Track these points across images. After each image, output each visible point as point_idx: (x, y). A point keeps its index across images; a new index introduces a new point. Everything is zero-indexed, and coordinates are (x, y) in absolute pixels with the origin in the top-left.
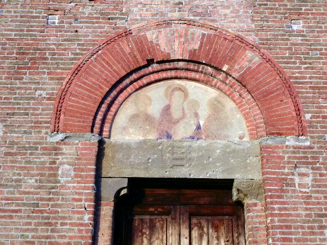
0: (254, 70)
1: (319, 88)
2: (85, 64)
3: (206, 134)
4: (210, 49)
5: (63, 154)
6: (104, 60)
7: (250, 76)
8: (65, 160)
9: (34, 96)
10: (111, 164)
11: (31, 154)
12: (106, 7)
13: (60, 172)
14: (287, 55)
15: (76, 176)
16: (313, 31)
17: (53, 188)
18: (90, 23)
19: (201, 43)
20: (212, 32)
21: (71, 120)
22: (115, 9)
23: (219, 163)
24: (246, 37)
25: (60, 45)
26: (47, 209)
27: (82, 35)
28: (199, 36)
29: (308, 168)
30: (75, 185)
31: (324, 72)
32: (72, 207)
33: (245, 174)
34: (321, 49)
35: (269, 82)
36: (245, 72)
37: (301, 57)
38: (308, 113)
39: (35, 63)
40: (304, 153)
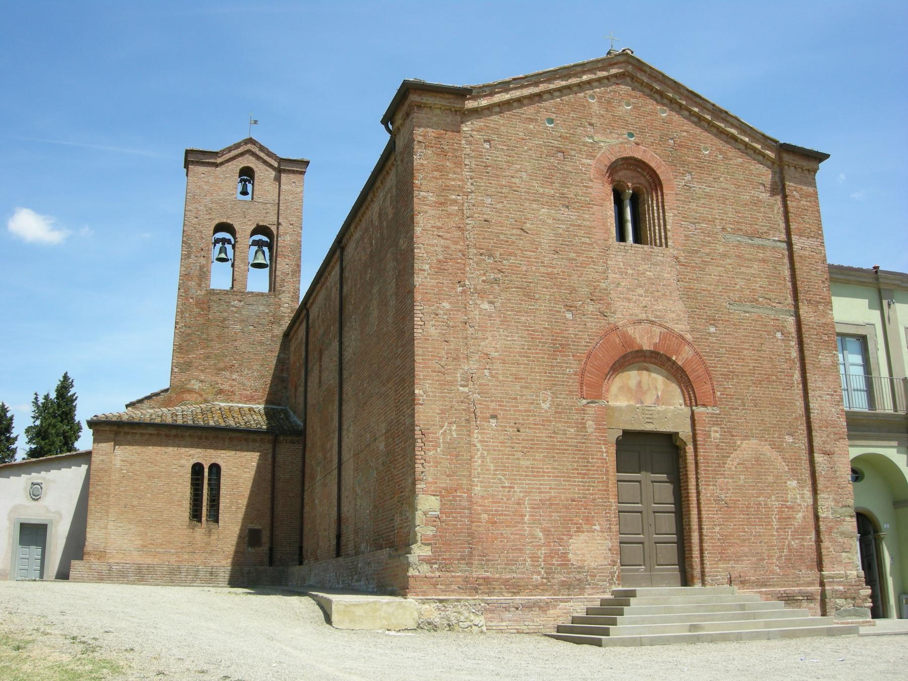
15: (596, 429)
33: (685, 431)
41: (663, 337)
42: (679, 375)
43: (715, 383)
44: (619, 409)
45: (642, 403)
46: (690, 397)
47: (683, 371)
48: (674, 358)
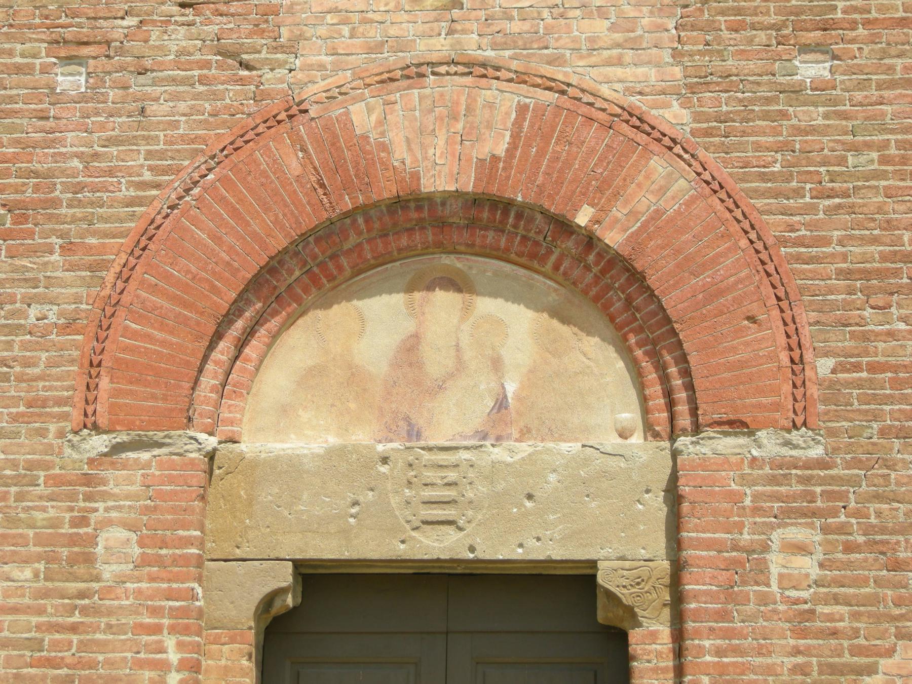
0: (671, 220)
1: (866, 275)
2: (167, 216)
3: (522, 424)
4: (541, 153)
5: (105, 496)
6: (222, 200)
7: (659, 242)
8: (114, 514)
9: (22, 322)
10: (243, 522)
11: (20, 497)
12: (232, 26)
13: (100, 550)
14: (777, 168)
15: (144, 561)
16: (861, 86)
17: (82, 595)
18: (183, 81)
19: (515, 137)
20: (551, 97)
21: (130, 393)
22: (258, 31)
23: (555, 512)
24: (653, 112)
25: (96, 156)
26: (70, 653)
27: (159, 123)
28: (508, 114)
29: (811, 526)
30: (144, 585)
31: (888, 222)
32: (135, 650)
33: (624, 551)
34: (886, 145)
35: (715, 261)
36: (645, 226)
37: (818, 173)
38: (826, 355)
39: (24, 219)
40: (806, 480)
41: (530, 130)
42: (615, 293)
43: (805, 317)
44: (288, 470)
45: (414, 433)
46: (668, 394)
47: (636, 277)
48: (582, 218)
